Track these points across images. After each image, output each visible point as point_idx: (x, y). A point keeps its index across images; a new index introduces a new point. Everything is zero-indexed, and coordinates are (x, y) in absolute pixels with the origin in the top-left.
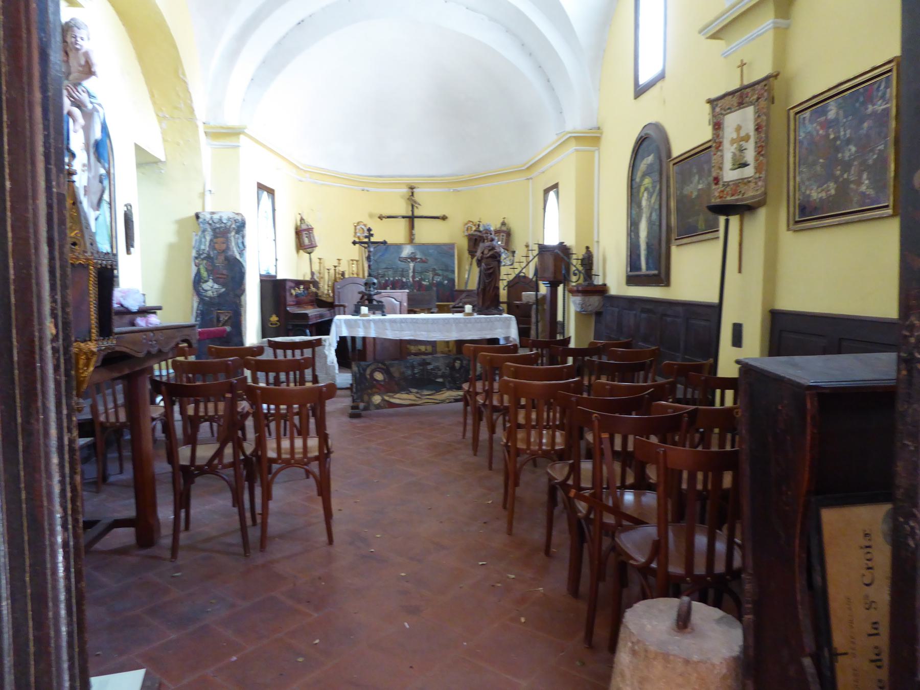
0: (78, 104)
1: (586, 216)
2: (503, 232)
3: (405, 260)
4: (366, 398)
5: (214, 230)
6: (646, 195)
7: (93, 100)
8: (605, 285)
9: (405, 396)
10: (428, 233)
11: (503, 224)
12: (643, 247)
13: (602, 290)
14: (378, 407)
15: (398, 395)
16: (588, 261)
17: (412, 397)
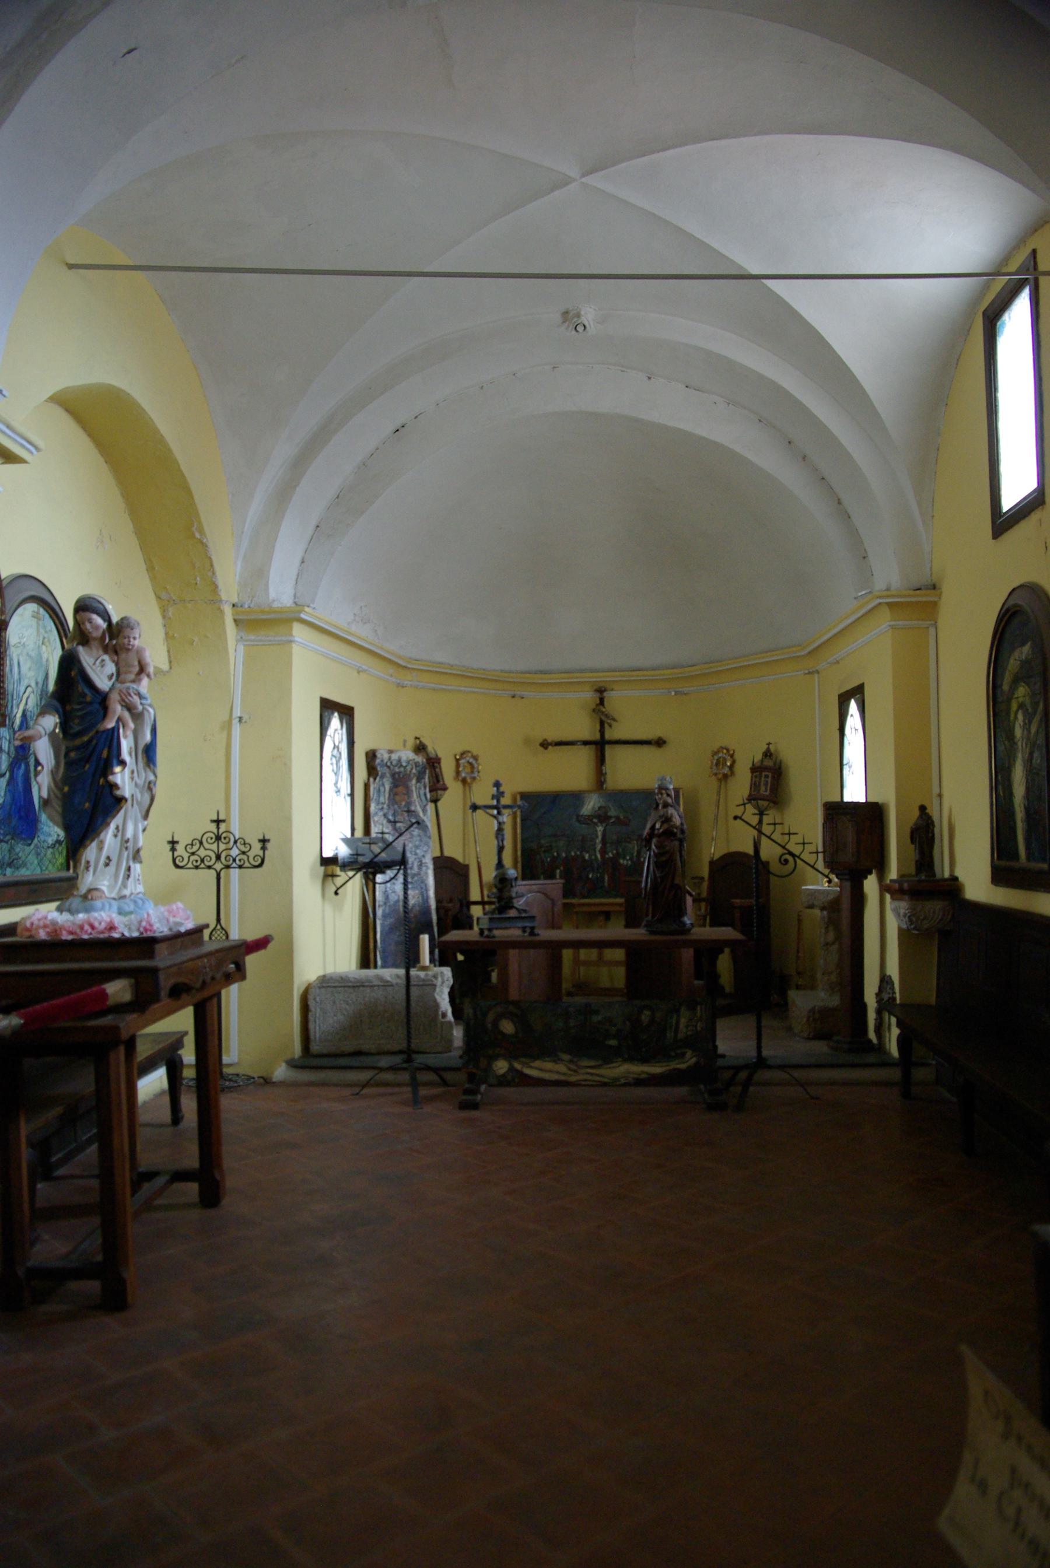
0: (129, 708)
1: (911, 748)
2: (766, 769)
3: (588, 820)
4: (483, 1062)
5: (393, 775)
6: (1020, 717)
7: (144, 702)
8: (956, 879)
9: (549, 1065)
10: (630, 771)
11: (767, 754)
12: (1020, 815)
13: (952, 889)
14: (503, 1081)
15: (537, 1063)
16: (924, 833)
17: (561, 1068)
